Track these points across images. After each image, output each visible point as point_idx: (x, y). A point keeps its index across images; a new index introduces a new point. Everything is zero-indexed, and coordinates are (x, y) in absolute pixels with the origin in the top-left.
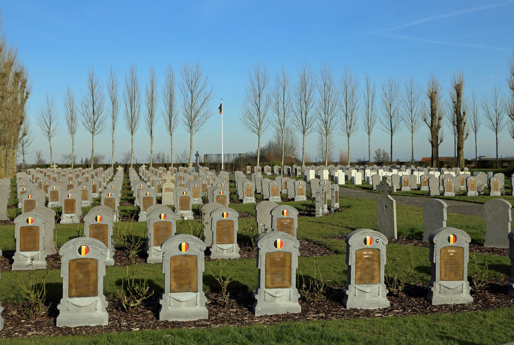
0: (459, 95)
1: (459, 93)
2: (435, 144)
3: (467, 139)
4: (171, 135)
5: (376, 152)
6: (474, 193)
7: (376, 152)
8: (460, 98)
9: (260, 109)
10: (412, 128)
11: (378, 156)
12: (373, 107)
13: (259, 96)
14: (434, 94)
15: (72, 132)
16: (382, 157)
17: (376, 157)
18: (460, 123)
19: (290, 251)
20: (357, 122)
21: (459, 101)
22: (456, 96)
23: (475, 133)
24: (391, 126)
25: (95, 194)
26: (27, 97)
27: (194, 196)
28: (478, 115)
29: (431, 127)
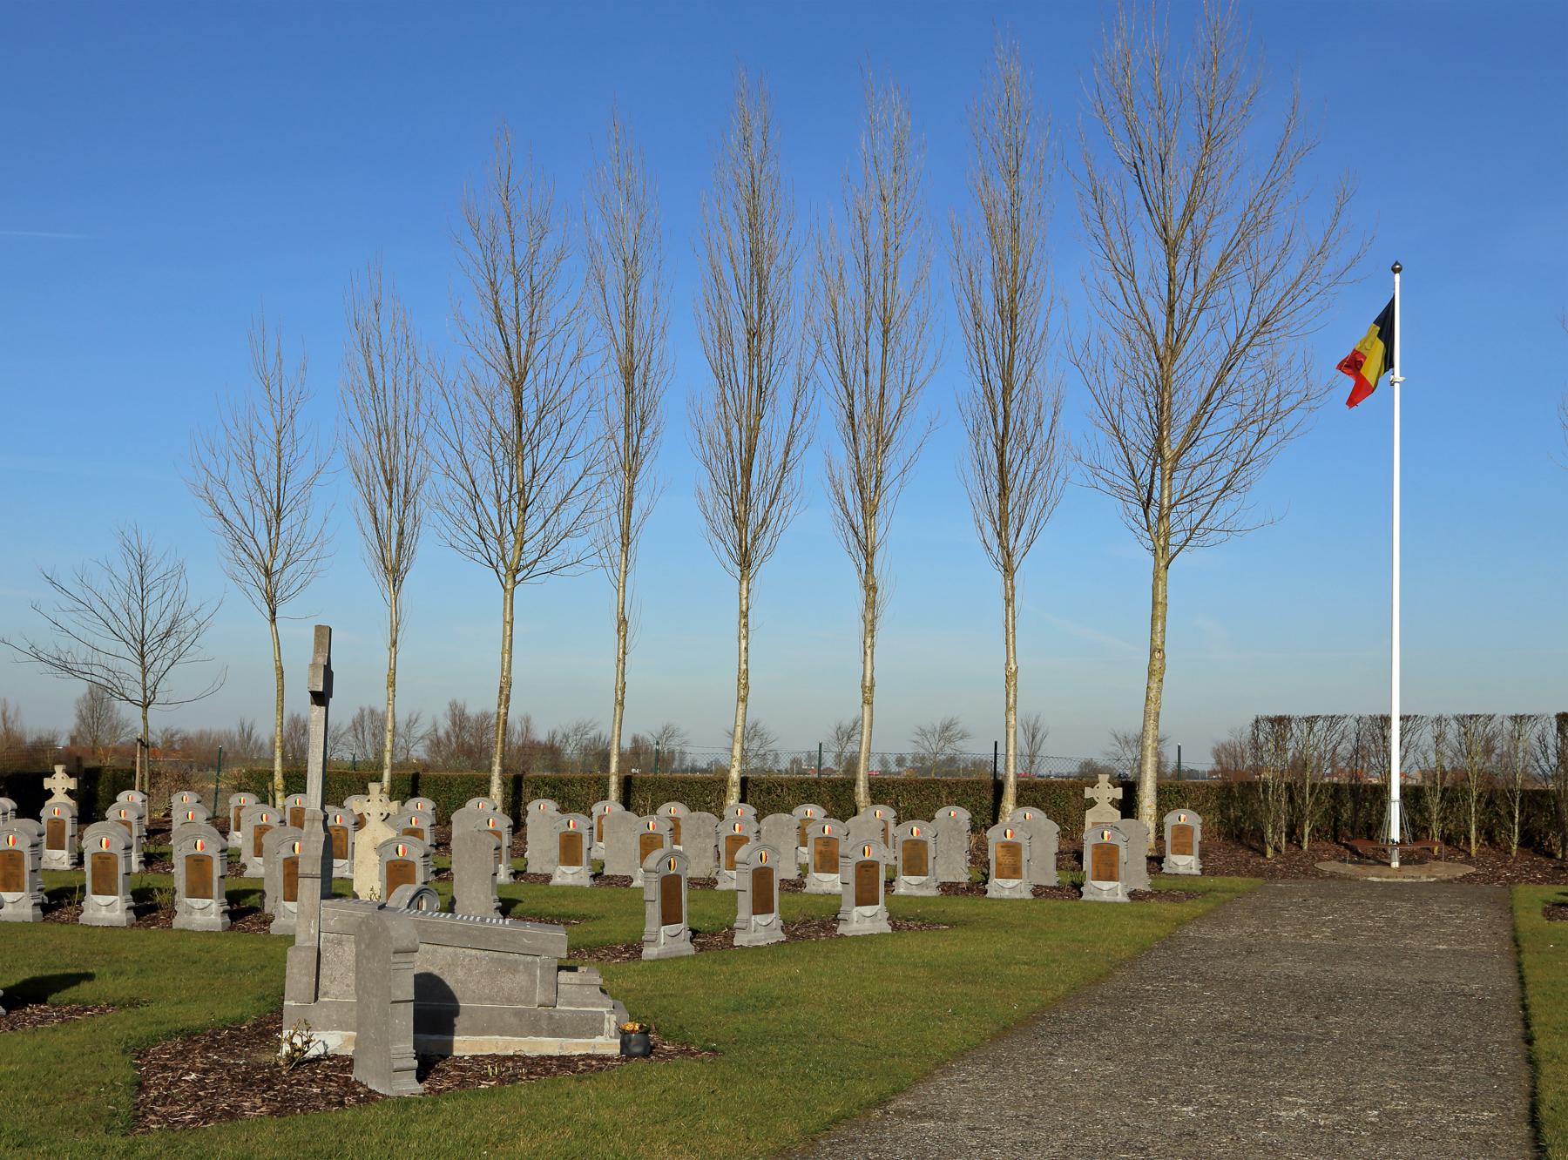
4: (1008, 570)
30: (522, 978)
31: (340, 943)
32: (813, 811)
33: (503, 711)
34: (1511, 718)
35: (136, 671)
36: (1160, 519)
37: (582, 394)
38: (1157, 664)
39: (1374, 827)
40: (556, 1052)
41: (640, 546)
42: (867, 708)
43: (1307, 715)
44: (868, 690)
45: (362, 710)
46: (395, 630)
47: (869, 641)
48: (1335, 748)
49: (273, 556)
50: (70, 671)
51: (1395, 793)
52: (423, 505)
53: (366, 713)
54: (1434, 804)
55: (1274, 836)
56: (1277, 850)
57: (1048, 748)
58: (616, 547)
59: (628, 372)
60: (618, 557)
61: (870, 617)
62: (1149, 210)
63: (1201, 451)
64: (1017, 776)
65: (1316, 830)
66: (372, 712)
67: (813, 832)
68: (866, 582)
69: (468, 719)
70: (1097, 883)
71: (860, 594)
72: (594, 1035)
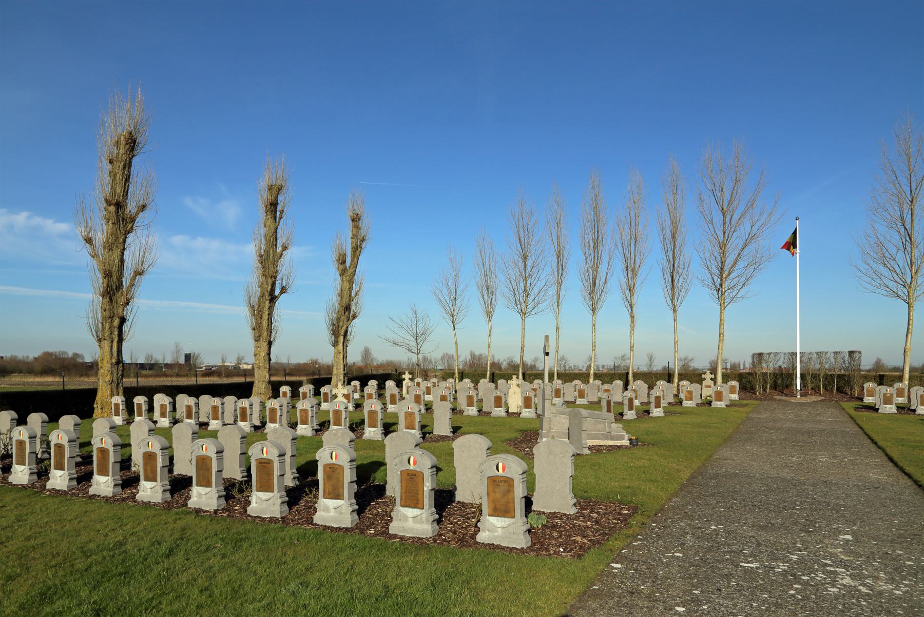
4: (675, 311)
9: (915, 230)
13: (912, 202)
19: (516, 517)
30: (602, 425)
31: (556, 416)
32: (577, 382)
33: (522, 354)
34: (833, 352)
35: (414, 344)
36: (722, 295)
37: (543, 263)
38: (722, 338)
40: (613, 444)
41: (563, 306)
42: (632, 352)
43: (768, 352)
44: (594, 346)
46: (490, 332)
47: (632, 333)
49: (454, 311)
50: (397, 345)
51: (798, 375)
52: (498, 293)
53: (445, 354)
54: (809, 378)
55: (758, 389)
56: (760, 393)
57: (655, 362)
58: (555, 306)
59: (558, 256)
60: (556, 310)
61: (632, 325)
62: (717, 203)
63: (733, 275)
64: (679, 371)
66: (447, 354)
67: (578, 388)
68: (631, 315)
69: (476, 356)
70: (716, 402)
71: (630, 319)
72: (622, 440)
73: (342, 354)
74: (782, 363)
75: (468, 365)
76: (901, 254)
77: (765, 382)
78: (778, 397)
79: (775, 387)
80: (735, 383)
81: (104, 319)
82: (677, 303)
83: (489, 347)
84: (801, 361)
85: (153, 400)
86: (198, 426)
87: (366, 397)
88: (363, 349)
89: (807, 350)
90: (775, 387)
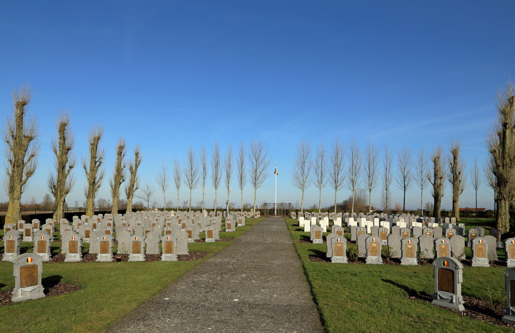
0: (455, 158)
1: (456, 157)
2: (437, 197)
3: (461, 194)
4: (242, 190)
5: (426, 204)
6: (377, 259)
7: (426, 204)
8: (457, 161)
9: (305, 170)
10: (422, 186)
11: (427, 207)
12: (390, 169)
14: (437, 159)
15: (178, 187)
16: (430, 207)
17: (426, 207)
18: (456, 181)
20: (378, 181)
21: (455, 163)
22: (453, 159)
23: (476, 190)
24: (404, 184)
25: (29, 237)
26: (139, 164)
27: (9, 251)
28: (479, 176)
29: (434, 185)
39: (274, 213)
45: (100, 199)
48: (505, 200)
54: (279, 211)
65: (269, 213)
66: (101, 199)
69: (120, 200)
73: (131, 202)
74: (271, 207)
75: (491, 215)
76: (301, 177)
77: (267, 212)
78: (271, 216)
79: (270, 213)
80: (259, 212)
81: (119, 196)
82: (243, 188)
83: (178, 199)
84: (277, 206)
85: (45, 221)
86: (20, 235)
87: (242, 210)
88: (45, 195)
89: (278, 202)
90: (270, 213)
